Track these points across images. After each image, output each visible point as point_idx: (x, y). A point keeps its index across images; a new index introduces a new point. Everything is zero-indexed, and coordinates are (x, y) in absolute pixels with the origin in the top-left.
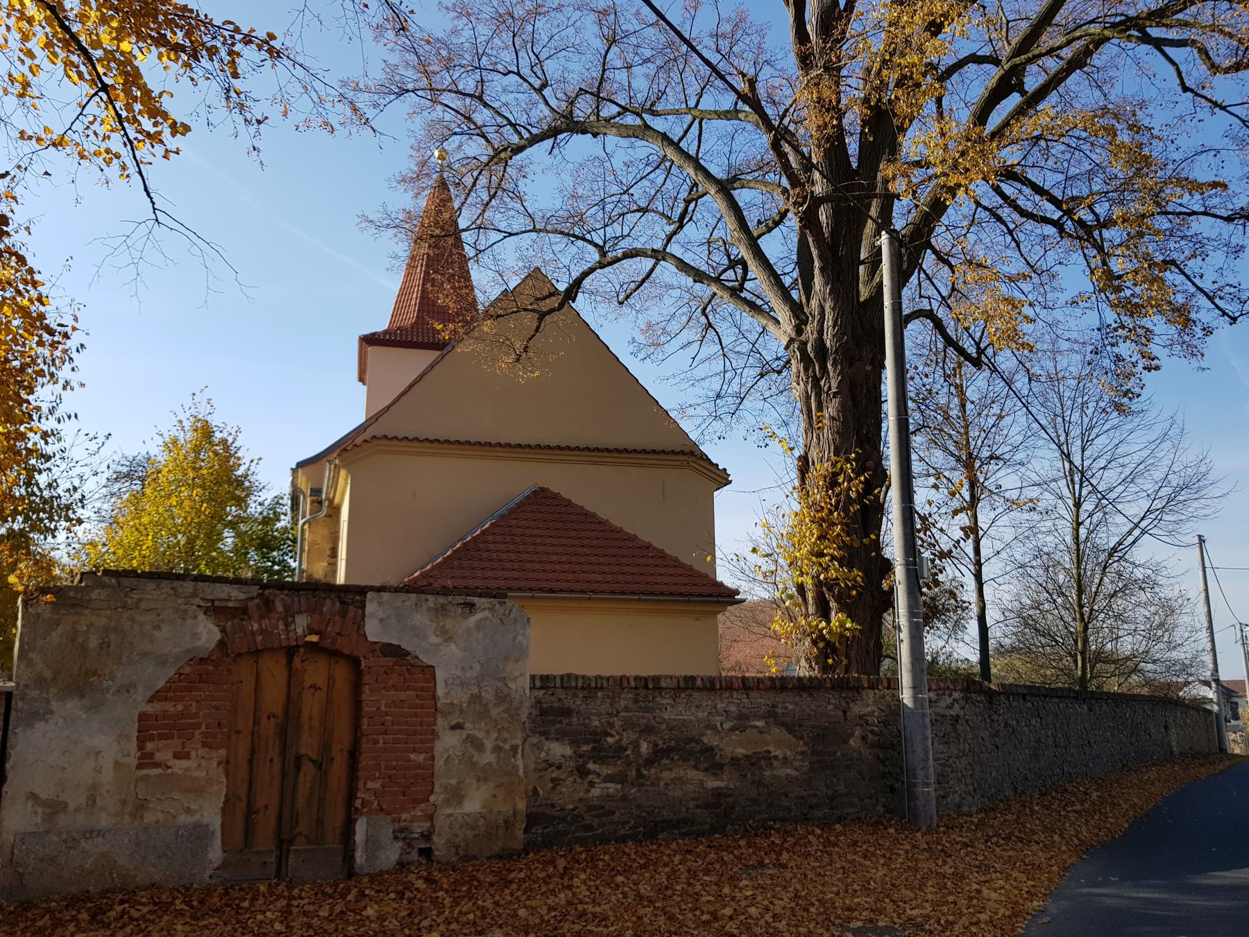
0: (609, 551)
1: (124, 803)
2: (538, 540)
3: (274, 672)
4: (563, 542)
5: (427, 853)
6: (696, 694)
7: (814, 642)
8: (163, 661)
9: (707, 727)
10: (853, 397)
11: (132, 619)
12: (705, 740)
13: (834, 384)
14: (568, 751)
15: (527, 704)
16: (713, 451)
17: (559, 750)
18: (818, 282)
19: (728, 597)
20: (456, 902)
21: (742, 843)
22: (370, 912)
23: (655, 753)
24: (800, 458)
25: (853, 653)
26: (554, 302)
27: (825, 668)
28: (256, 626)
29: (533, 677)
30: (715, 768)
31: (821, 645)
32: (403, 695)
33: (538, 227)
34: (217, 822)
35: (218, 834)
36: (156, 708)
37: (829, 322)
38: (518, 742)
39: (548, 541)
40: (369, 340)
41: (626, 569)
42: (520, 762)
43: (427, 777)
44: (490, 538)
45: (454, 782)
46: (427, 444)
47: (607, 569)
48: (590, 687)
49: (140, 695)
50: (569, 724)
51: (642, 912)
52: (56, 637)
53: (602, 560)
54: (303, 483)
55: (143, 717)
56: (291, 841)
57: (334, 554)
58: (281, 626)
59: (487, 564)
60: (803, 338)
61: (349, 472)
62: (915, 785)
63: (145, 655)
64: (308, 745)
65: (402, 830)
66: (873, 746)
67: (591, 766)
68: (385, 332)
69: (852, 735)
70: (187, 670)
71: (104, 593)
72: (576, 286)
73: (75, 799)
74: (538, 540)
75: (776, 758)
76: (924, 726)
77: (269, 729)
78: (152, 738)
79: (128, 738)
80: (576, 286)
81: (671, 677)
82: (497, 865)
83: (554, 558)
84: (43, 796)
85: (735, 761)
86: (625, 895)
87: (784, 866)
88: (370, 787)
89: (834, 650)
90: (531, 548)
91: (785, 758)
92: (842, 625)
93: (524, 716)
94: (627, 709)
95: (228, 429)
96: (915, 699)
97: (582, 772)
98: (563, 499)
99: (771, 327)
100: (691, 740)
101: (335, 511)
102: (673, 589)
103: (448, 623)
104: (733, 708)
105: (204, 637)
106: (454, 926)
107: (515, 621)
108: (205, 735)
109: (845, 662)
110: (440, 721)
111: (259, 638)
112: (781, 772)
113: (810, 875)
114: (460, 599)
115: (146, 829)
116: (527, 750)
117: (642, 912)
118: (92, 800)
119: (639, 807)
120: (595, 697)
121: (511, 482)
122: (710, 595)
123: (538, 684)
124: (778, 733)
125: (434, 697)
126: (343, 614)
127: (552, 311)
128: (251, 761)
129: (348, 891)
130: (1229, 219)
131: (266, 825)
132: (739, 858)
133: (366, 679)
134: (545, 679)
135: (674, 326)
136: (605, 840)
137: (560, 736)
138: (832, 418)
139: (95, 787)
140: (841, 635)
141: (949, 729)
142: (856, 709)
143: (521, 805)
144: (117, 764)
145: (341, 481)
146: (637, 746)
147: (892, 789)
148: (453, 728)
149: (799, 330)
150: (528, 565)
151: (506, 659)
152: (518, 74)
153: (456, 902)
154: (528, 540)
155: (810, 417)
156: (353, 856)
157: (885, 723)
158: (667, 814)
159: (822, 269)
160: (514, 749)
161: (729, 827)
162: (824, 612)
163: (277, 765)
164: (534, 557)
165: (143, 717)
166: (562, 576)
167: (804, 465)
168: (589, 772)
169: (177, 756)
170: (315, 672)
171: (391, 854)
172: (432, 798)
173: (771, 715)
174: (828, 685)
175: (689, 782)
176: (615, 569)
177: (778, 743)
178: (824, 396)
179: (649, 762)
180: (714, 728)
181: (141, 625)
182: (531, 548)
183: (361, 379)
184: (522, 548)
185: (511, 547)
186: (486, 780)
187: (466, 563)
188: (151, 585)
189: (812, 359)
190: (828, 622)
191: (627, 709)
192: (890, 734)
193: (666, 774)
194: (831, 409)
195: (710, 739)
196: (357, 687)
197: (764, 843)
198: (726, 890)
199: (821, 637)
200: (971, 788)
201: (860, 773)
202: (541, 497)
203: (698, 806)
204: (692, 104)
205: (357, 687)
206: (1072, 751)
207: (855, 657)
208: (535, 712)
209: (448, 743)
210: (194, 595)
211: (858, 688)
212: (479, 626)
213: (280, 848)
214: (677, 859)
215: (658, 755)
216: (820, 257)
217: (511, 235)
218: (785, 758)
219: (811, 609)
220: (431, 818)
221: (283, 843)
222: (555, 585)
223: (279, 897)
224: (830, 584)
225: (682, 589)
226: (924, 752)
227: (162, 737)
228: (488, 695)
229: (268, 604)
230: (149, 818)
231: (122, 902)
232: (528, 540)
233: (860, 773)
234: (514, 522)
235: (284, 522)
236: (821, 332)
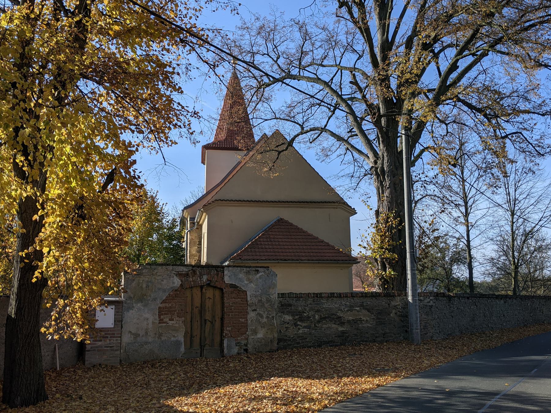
0: (307, 244)
1: (156, 334)
2: (280, 240)
3: (197, 292)
4: (290, 240)
5: (246, 350)
6: (335, 299)
7: (380, 279)
8: (164, 291)
9: (339, 310)
10: (395, 189)
11: (155, 278)
12: (338, 314)
13: (388, 184)
14: (291, 318)
15: (277, 303)
16: (350, 202)
17: (288, 318)
18: (381, 145)
19: (355, 261)
20: (257, 363)
21: (350, 348)
22: (231, 365)
23: (321, 319)
24: (376, 211)
25: (395, 283)
26: (284, 147)
27: (384, 289)
28: (191, 279)
29: (278, 294)
30: (342, 324)
31: (382, 281)
32: (237, 300)
33: (277, 116)
34: (183, 340)
35: (183, 344)
36: (164, 305)
37: (385, 161)
38: (274, 315)
39: (284, 240)
40: (206, 147)
41: (314, 251)
42: (275, 322)
43: (245, 326)
44: (262, 240)
45: (254, 328)
46: (236, 202)
47: (306, 251)
48: (298, 297)
49: (159, 301)
50: (291, 309)
51: (313, 365)
52: (134, 284)
53: (304, 247)
54: (186, 214)
55: (159, 308)
56: (204, 346)
57: (200, 243)
58: (199, 279)
59: (261, 250)
60: (377, 166)
61: (207, 214)
62: (413, 329)
63: (159, 289)
64: (208, 316)
65: (238, 343)
66: (399, 316)
67: (299, 323)
68: (213, 143)
69: (392, 312)
70: (172, 293)
71: (147, 270)
72: (293, 139)
73: (142, 333)
74: (280, 240)
75: (363, 320)
76: (416, 309)
77: (196, 311)
78: (162, 315)
79: (156, 314)
80: (293, 139)
81: (326, 293)
82: (268, 354)
83: (286, 247)
84: (133, 332)
85: (349, 321)
86: (309, 361)
87: (362, 355)
88: (227, 329)
89: (388, 282)
90: (277, 243)
91: (367, 320)
92: (390, 273)
93: (276, 307)
94: (311, 304)
95: (153, 191)
96: (413, 299)
97: (296, 325)
98: (289, 223)
99: (366, 159)
100: (333, 314)
101: (200, 227)
102: (332, 258)
103: (250, 277)
104: (348, 303)
105: (176, 283)
106: (256, 369)
107: (272, 275)
108: (178, 313)
109: (392, 286)
110: (249, 308)
111: (192, 283)
112: (365, 325)
113: (91, 234)
114: (254, 269)
115: (162, 342)
116: (277, 317)
117: (313, 365)
118: (147, 333)
119: (315, 337)
120: (300, 300)
121: (269, 215)
122: (346, 260)
123: (280, 296)
124: (365, 312)
125: (247, 301)
126: (218, 275)
127: (283, 151)
128: (191, 321)
129: (224, 360)
130: (543, 115)
131: (197, 340)
132: (348, 353)
133: (225, 295)
134: (283, 294)
135: (334, 148)
136: (304, 347)
137: (288, 313)
138: (387, 197)
139: (147, 329)
140: (390, 277)
141: (429, 310)
142: (393, 303)
143: (276, 335)
144: (153, 323)
145: (203, 217)
146: (314, 317)
147: (406, 331)
148: (253, 311)
149: (376, 162)
150: (276, 250)
151: (270, 288)
152: (268, 55)
153: (257, 363)
154: (276, 240)
155: (379, 196)
156: (223, 351)
157: (404, 308)
158: (325, 339)
159: (383, 141)
160: (273, 317)
161: (347, 344)
162: (384, 268)
163: (199, 323)
164: (279, 247)
165: (159, 308)
166: (289, 254)
167: (377, 213)
168: (298, 325)
169: (170, 320)
170: (209, 293)
171: (235, 350)
172: (247, 333)
173: (362, 306)
174: (383, 295)
175: (335, 328)
176: (310, 251)
177: (364, 315)
178: (384, 188)
179: (319, 322)
180: (341, 310)
181: (158, 280)
182: (277, 243)
183: (203, 162)
184: (274, 243)
185: (270, 243)
186: (264, 327)
187: (253, 250)
188: (160, 268)
189: (379, 174)
190: (386, 272)
191: (311, 304)
192: (404, 313)
193: (324, 326)
194: (387, 193)
195: (340, 314)
196: (222, 298)
197: (358, 348)
198: (341, 360)
199: (383, 277)
200: (438, 331)
201: (394, 325)
202: (280, 222)
203: (336, 337)
204: (338, 63)
205: (222, 298)
206: (494, 319)
207: (394, 286)
208: (280, 305)
209: (252, 315)
210: (173, 270)
211: (394, 296)
212: (260, 277)
213: (201, 348)
214: (327, 353)
215: (322, 319)
216: (381, 137)
217: (266, 120)
218: (367, 320)
219: (380, 268)
220: (247, 339)
221: (202, 347)
222: (286, 258)
223: (204, 361)
224: (387, 259)
225: (335, 258)
226: (416, 318)
227: (165, 314)
228: (264, 300)
229: (194, 272)
230: (163, 338)
231: (159, 362)
232: (276, 240)
233: (394, 325)
234: (270, 233)
235: (177, 229)
236: (383, 164)
